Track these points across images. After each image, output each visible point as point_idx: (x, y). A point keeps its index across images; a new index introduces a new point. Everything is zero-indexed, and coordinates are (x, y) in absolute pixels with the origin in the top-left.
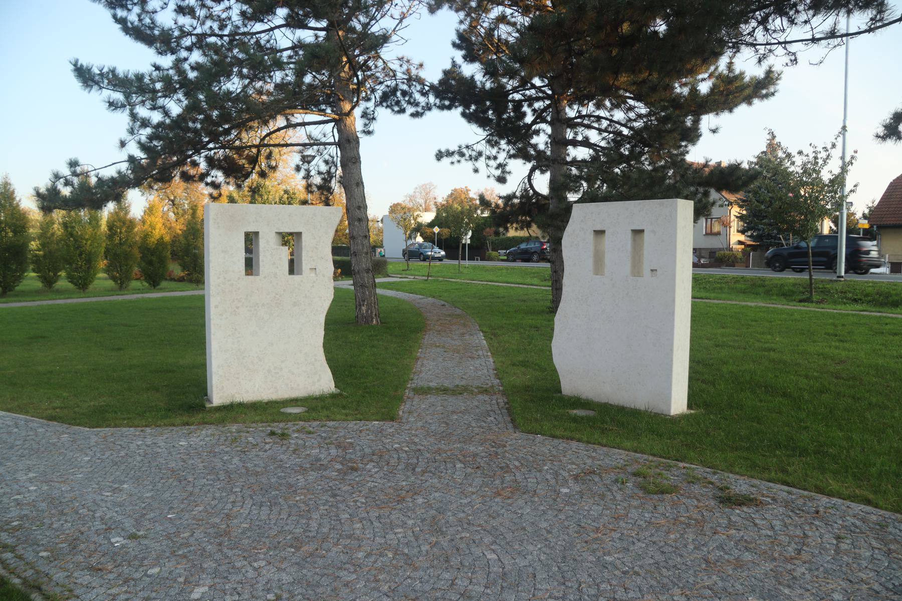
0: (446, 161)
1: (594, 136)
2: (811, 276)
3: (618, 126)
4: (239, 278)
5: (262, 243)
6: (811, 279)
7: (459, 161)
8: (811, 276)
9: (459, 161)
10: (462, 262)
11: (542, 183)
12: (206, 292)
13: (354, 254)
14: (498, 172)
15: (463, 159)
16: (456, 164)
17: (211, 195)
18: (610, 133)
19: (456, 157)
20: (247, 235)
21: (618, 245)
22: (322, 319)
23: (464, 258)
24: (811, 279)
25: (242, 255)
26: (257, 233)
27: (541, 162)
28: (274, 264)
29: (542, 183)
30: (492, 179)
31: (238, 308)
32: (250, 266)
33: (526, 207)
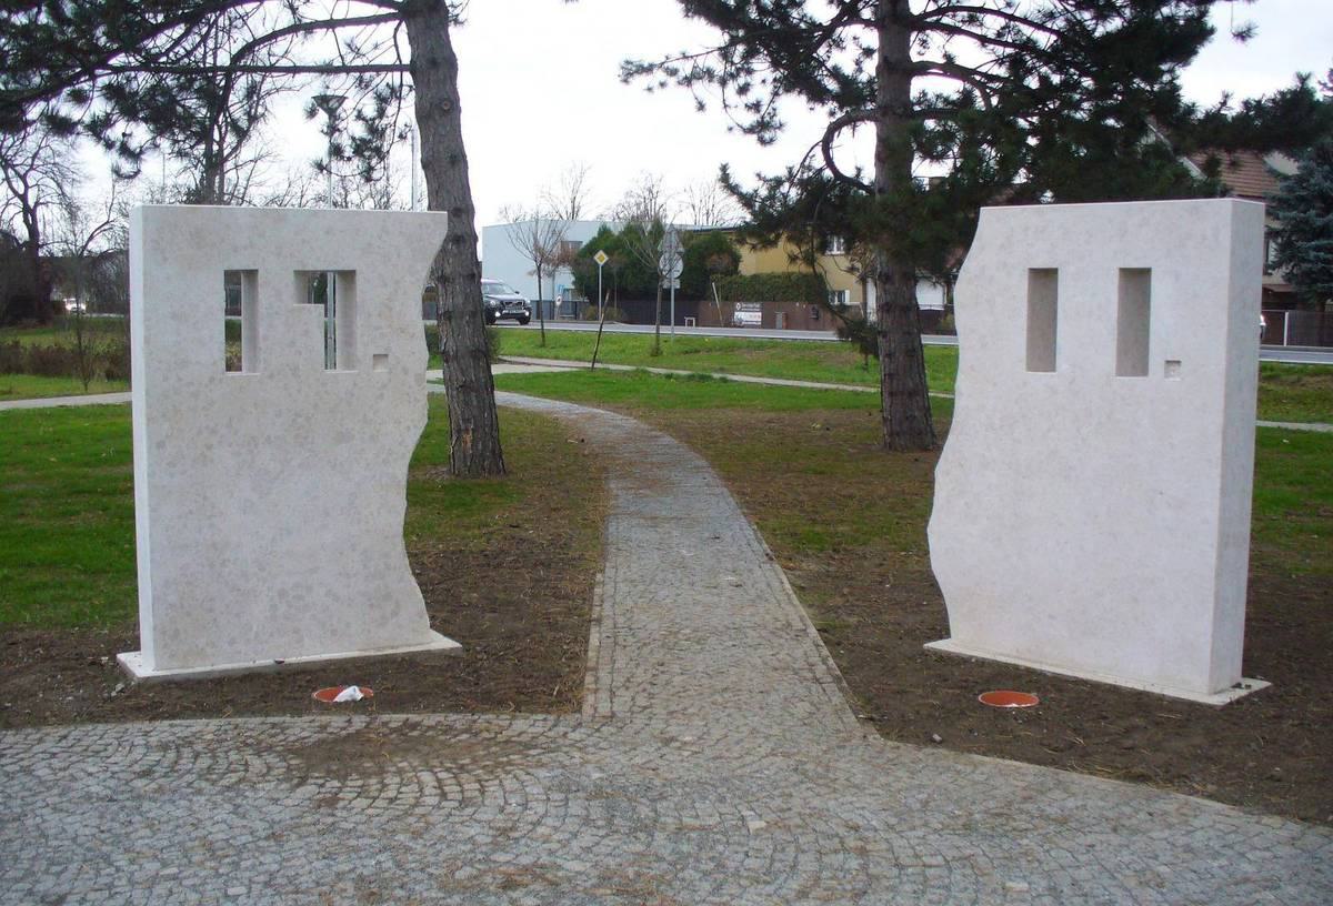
0: (640, 81)
1: (969, 53)
2: (658, 330)
3: (1027, 30)
4: (212, 380)
5: (264, 295)
6: (658, 333)
7: (662, 85)
8: (658, 330)
9: (662, 85)
10: (664, 330)
11: (858, 152)
12: (1255, 354)
13: (462, 316)
14: (751, 118)
15: (672, 81)
16: (658, 91)
17: (117, 171)
18: (1006, 44)
19: (659, 75)
20: (232, 277)
21: (1089, 310)
22: (401, 471)
23: (666, 322)
24: (658, 333)
25: (221, 319)
26: (252, 274)
27: (851, 99)
28: (293, 344)
29: (858, 152)
30: (738, 132)
31: (209, 447)
32: (1042, 349)
33: (819, 208)
